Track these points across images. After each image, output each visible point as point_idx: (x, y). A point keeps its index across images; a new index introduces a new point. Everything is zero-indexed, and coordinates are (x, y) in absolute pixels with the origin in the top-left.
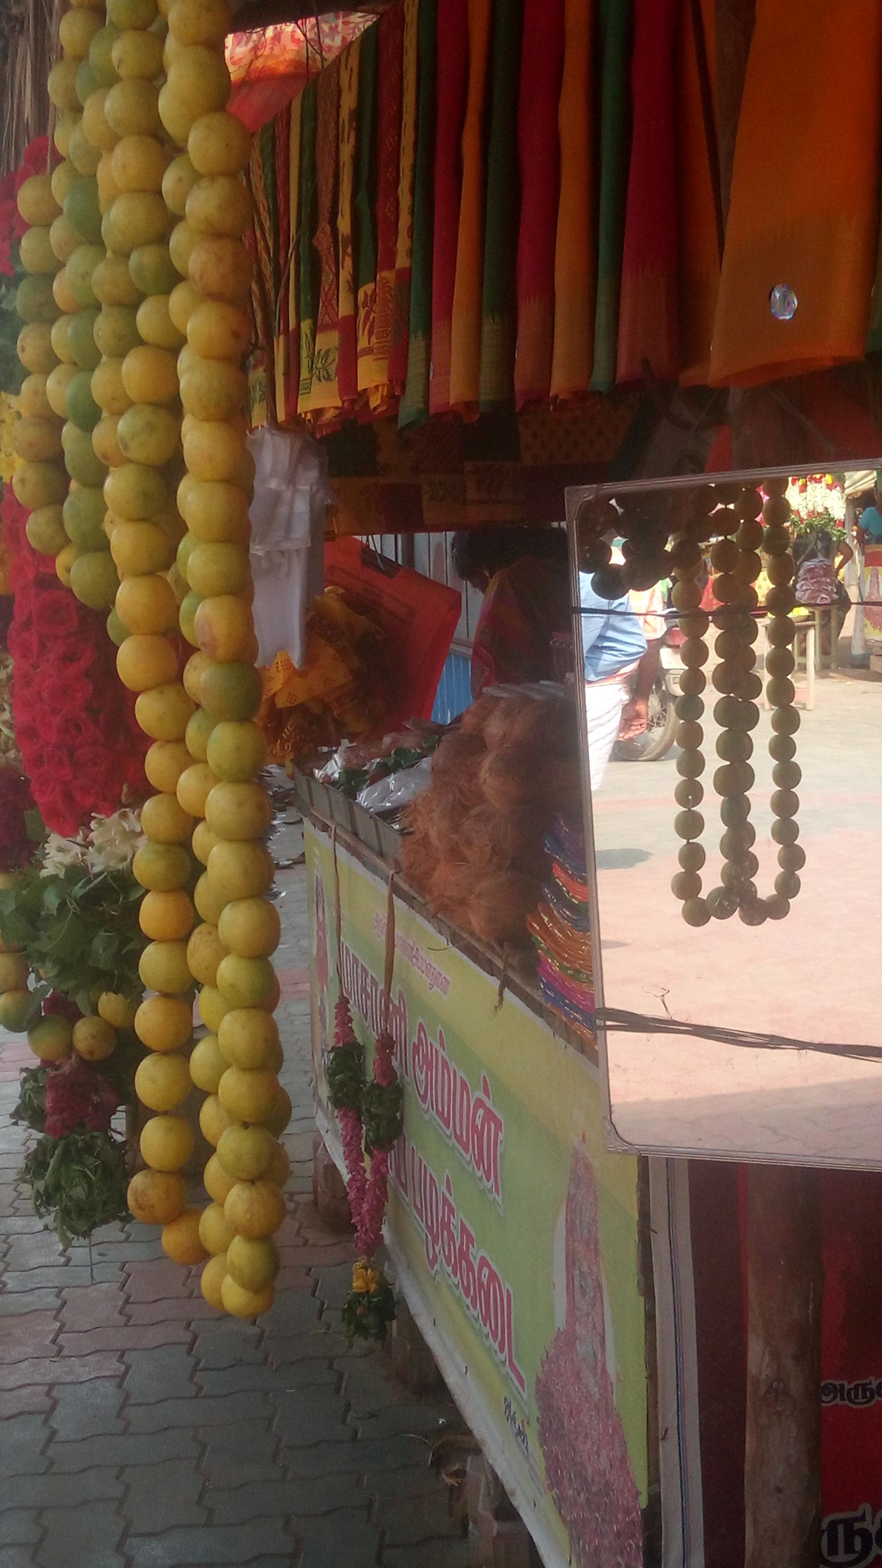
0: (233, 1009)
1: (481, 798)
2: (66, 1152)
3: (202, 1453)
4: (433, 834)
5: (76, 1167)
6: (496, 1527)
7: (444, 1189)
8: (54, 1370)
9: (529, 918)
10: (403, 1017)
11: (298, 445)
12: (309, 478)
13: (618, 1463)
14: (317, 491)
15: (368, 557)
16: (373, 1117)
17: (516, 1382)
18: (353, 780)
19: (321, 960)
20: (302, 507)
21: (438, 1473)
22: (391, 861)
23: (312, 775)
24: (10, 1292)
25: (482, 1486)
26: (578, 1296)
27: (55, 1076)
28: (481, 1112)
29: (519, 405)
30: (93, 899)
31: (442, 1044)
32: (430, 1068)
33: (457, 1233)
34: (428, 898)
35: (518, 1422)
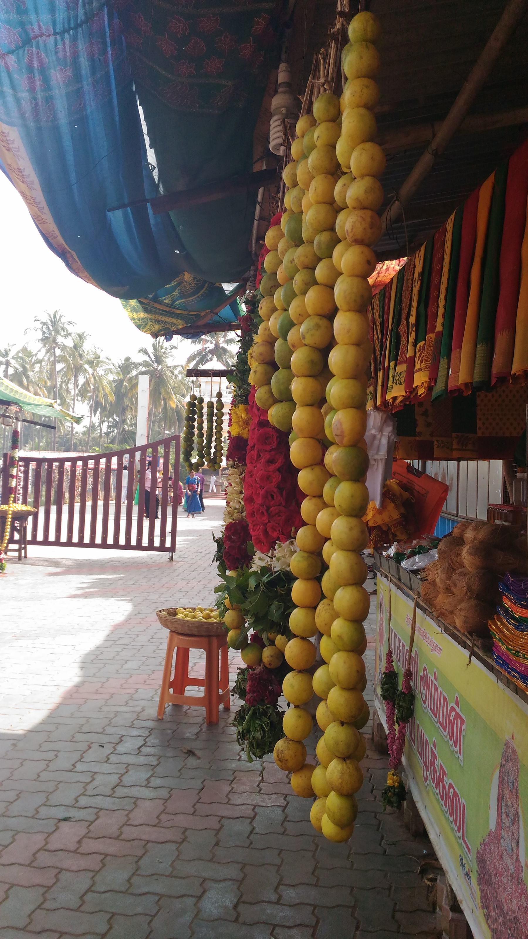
0: (339, 650)
1: (462, 565)
2: (254, 713)
3: (316, 850)
4: (438, 580)
5: (258, 722)
6: (451, 915)
7: (432, 746)
8: (257, 799)
9: (489, 622)
10: (416, 663)
11: (385, 416)
12: (388, 430)
13: (523, 910)
14: (391, 436)
15: (410, 469)
16: (400, 707)
17: (467, 851)
18: (399, 557)
19: (381, 634)
20: (384, 442)
21: (422, 878)
22: (416, 592)
23: (382, 554)
24: (243, 761)
25: (445, 892)
26: (504, 816)
27: (252, 674)
28: (453, 713)
29: (494, 381)
30: (271, 584)
31: (435, 679)
32: (428, 688)
33: (438, 769)
34: (433, 609)
35: (467, 869)
